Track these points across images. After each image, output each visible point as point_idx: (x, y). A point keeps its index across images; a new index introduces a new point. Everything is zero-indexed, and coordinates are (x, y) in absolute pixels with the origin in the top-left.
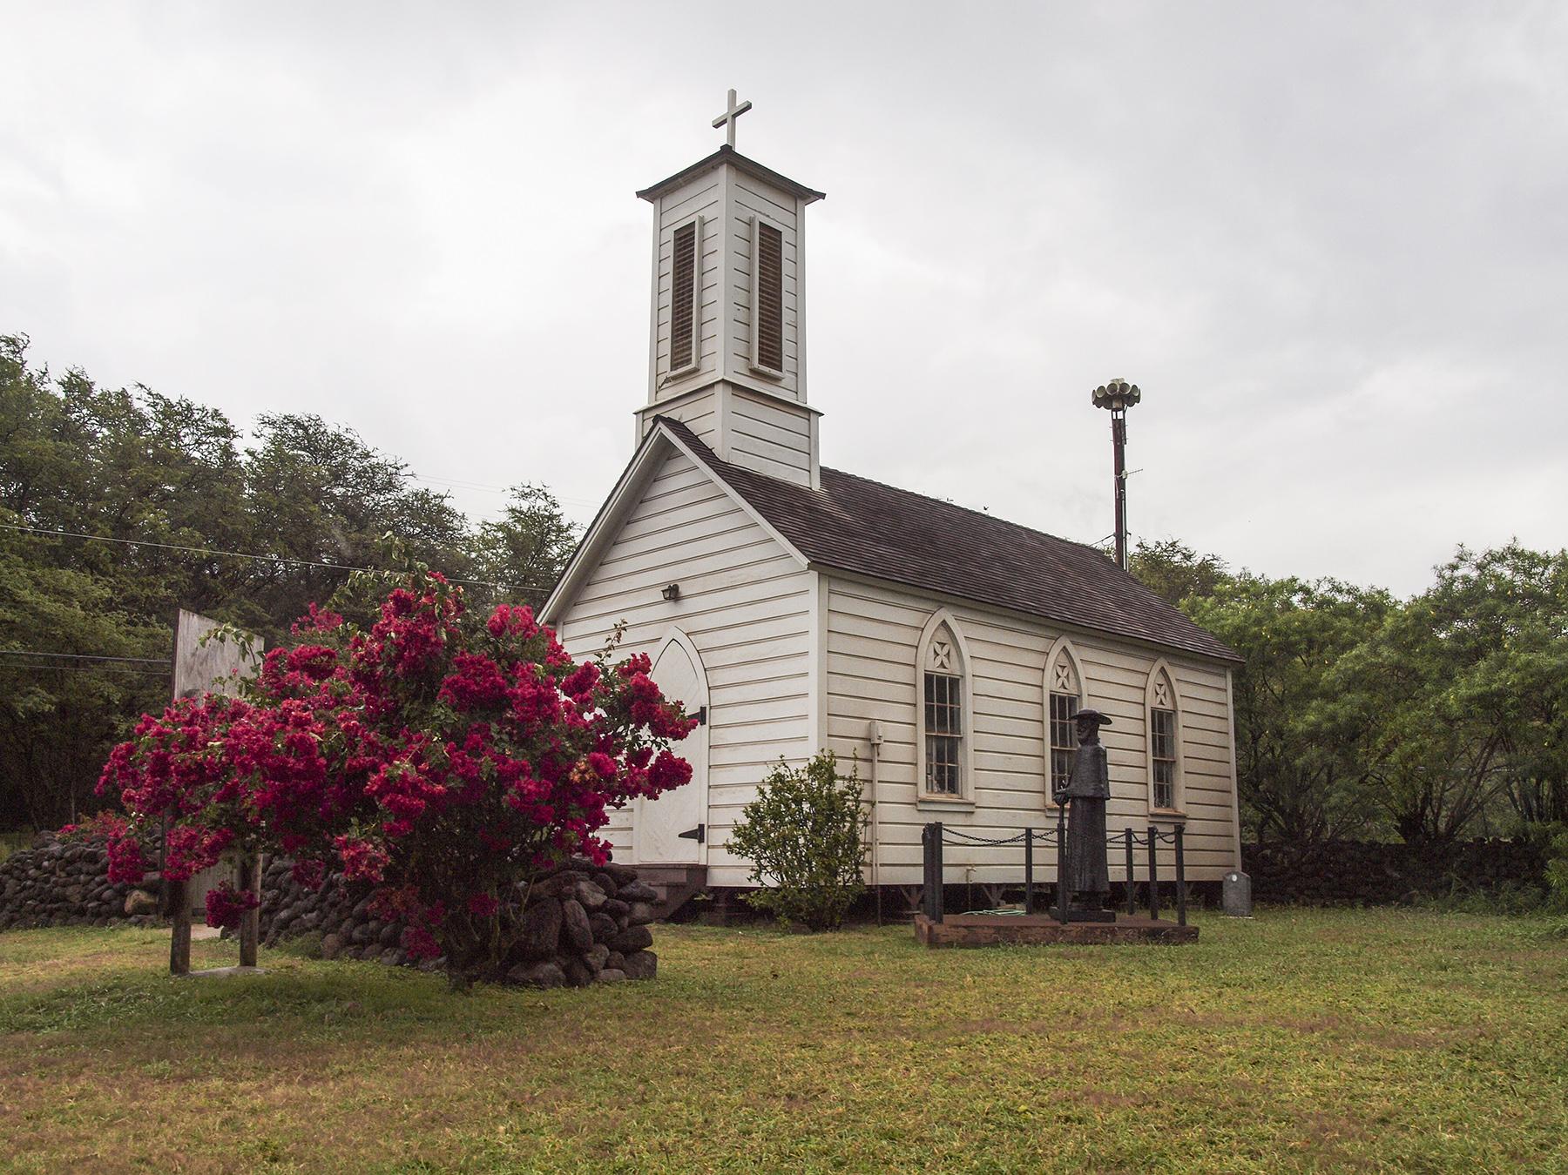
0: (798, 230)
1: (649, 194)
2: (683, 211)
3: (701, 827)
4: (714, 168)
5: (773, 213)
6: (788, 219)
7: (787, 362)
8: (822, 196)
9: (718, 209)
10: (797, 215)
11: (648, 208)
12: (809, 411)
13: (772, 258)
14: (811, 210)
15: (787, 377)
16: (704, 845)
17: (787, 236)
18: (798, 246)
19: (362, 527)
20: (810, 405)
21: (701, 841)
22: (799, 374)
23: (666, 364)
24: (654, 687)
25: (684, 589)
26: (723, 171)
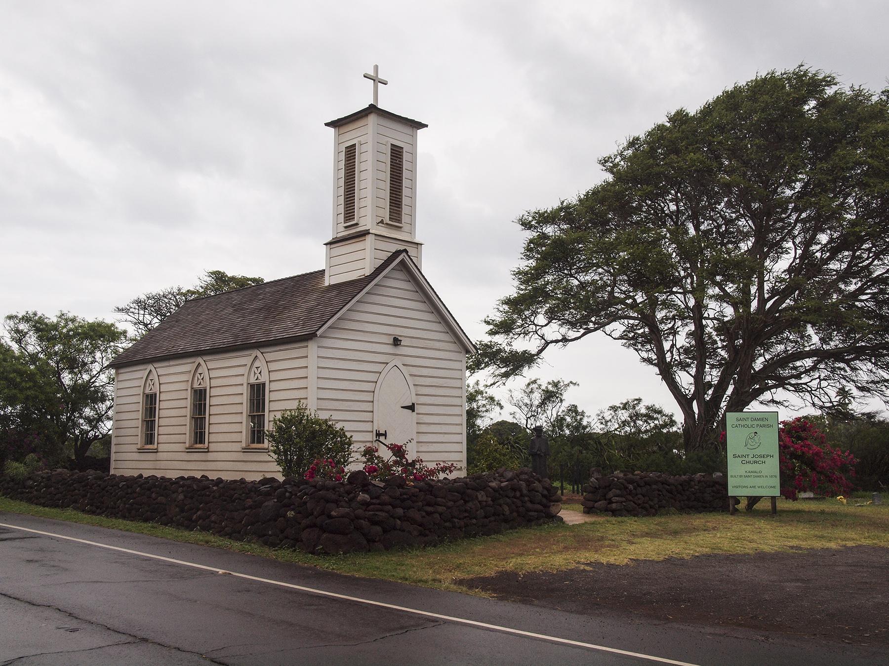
0: (414, 145)
1: (335, 124)
2: (353, 135)
3: (413, 404)
4: (367, 115)
5: (398, 136)
6: (408, 139)
7: (405, 218)
8: (427, 126)
9: (370, 140)
10: (414, 137)
11: (331, 130)
12: (417, 244)
13: (398, 163)
14: (420, 132)
15: (406, 227)
16: (414, 413)
17: (406, 148)
18: (414, 154)
19: (845, 397)
20: (417, 240)
21: (413, 411)
22: (412, 224)
23: (342, 217)
24: (650, 134)
25: (391, 341)
26: (372, 119)
